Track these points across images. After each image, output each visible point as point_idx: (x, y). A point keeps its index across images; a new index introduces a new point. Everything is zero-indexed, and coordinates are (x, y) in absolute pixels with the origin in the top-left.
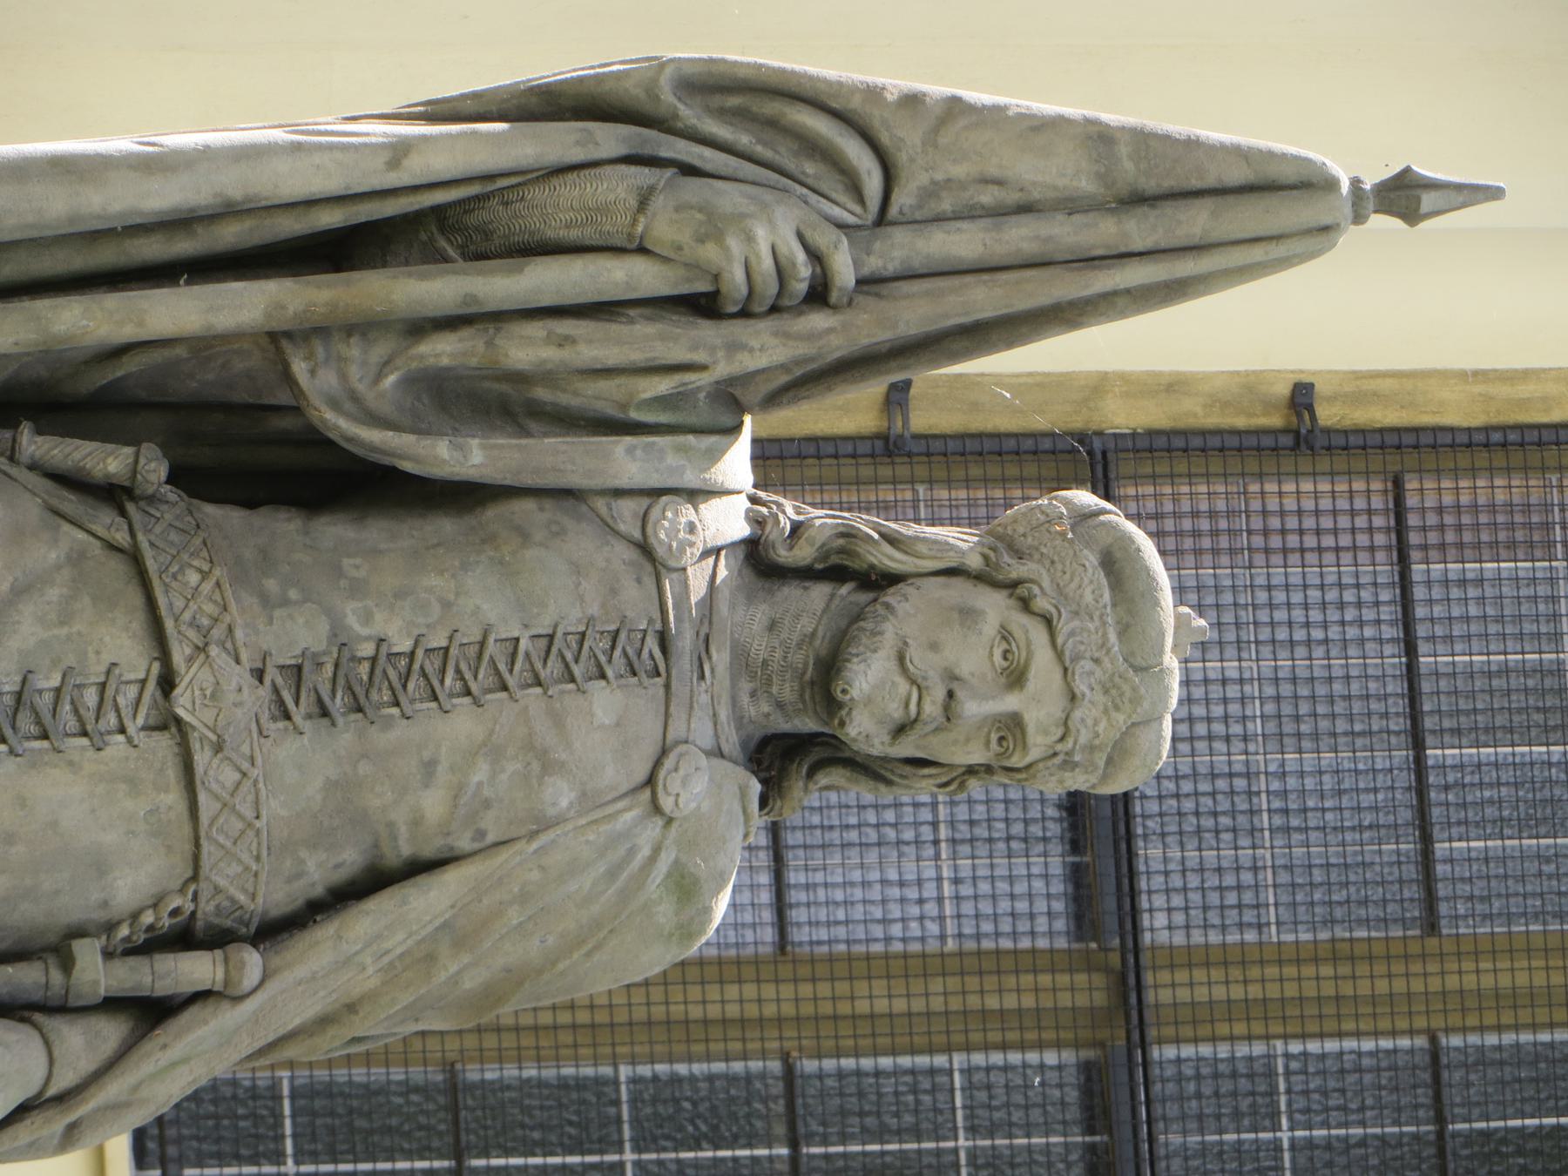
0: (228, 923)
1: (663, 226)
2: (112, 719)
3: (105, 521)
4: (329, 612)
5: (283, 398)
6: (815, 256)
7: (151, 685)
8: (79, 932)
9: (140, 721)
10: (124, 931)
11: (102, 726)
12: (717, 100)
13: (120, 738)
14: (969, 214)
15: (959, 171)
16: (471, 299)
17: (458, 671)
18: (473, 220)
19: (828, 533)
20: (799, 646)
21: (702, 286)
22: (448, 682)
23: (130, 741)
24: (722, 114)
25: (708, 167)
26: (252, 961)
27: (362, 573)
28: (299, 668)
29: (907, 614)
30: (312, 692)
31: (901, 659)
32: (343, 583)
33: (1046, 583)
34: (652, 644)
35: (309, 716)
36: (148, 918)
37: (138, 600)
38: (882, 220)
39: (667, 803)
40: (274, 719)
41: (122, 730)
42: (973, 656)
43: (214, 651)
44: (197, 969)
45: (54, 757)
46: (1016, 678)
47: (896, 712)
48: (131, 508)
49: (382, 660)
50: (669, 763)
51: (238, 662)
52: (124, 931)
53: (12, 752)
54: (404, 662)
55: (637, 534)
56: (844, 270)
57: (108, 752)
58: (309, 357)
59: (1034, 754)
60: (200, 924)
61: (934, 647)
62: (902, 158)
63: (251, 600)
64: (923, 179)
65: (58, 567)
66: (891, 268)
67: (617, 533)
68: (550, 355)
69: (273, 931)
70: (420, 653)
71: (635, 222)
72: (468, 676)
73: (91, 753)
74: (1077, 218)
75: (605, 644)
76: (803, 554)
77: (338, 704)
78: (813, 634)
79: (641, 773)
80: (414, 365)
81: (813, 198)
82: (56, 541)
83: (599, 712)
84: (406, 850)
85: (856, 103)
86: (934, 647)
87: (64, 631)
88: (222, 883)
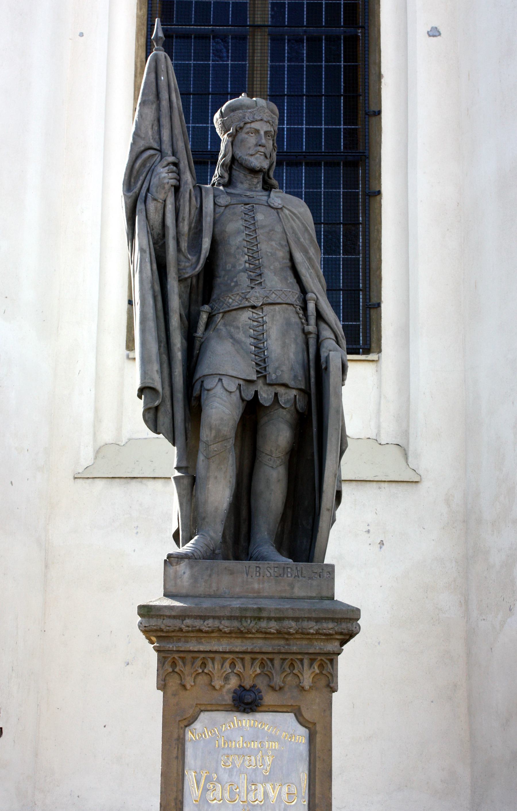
0: (301, 299)
1: (161, 196)
2: (260, 319)
3: (219, 318)
4: (239, 272)
5: (189, 281)
6: (168, 164)
7: (254, 311)
8: (303, 330)
9: (261, 314)
10: (303, 321)
11: (262, 322)
12: (132, 184)
13: (264, 318)
14: (159, 132)
15: (150, 133)
16: (173, 238)
17: (252, 247)
18: (156, 237)
19: (222, 169)
20: (246, 177)
21: (173, 189)
22: (255, 249)
23: (265, 316)
24: (136, 182)
25: (147, 186)
26: (310, 295)
27: (230, 265)
28: (251, 279)
29: (240, 154)
30: (257, 277)
31: (252, 155)
32: (233, 269)
33: (237, 124)
34: (247, 206)
35: (261, 278)
36: (301, 315)
37: (234, 312)
38: (160, 151)
39: (280, 206)
40: (261, 285)
41: (263, 317)
42: (252, 140)
43: (247, 297)
44: (311, 306)
45: (268, 332)
46: (257, 131)
47: (262, 157)
48: (214, 313)
49: (250, 262)
50: (272, 205)
51: (249, 292)
52: (303, 321)
53: (266, 341)
54: (250, 258)
55: (223, 208)
56: (171, 159)
57: (267, 321)
58: (184, 273)
59: (272, 130)
60: (301, 305)
61: (249, 148)
62: (147, 145)
63: (236, 289)
64: (152, 141)
65: (227, 329)
66: (171, 149)
67: (223, 213)
68: (186, 222)
69: (304, 291)
70: (248, 254)
71: (159, 202)
72: (253, 244)
73: (267, 324)
74: (161, 109)
75: (247, 216)
76: (226, 175)
77: (258, 271)
78: (244, 174)
79: (274, 212)
80: (186, 251)
81: (155, 164)
82: (220, 329)
83: (261, 219)
84: (288, 261)
85: (134, 154)
86: (249, 148)
87: (241, 328)
88: (294, 299)
